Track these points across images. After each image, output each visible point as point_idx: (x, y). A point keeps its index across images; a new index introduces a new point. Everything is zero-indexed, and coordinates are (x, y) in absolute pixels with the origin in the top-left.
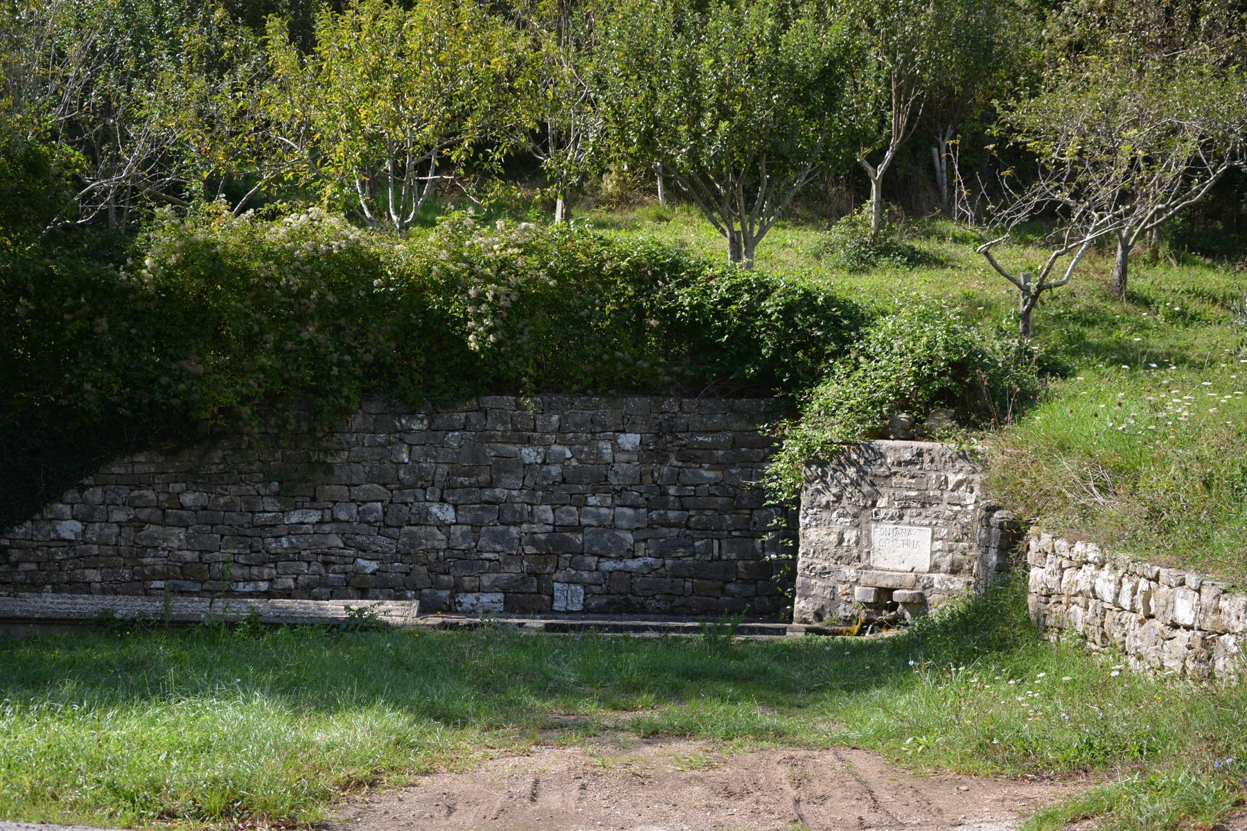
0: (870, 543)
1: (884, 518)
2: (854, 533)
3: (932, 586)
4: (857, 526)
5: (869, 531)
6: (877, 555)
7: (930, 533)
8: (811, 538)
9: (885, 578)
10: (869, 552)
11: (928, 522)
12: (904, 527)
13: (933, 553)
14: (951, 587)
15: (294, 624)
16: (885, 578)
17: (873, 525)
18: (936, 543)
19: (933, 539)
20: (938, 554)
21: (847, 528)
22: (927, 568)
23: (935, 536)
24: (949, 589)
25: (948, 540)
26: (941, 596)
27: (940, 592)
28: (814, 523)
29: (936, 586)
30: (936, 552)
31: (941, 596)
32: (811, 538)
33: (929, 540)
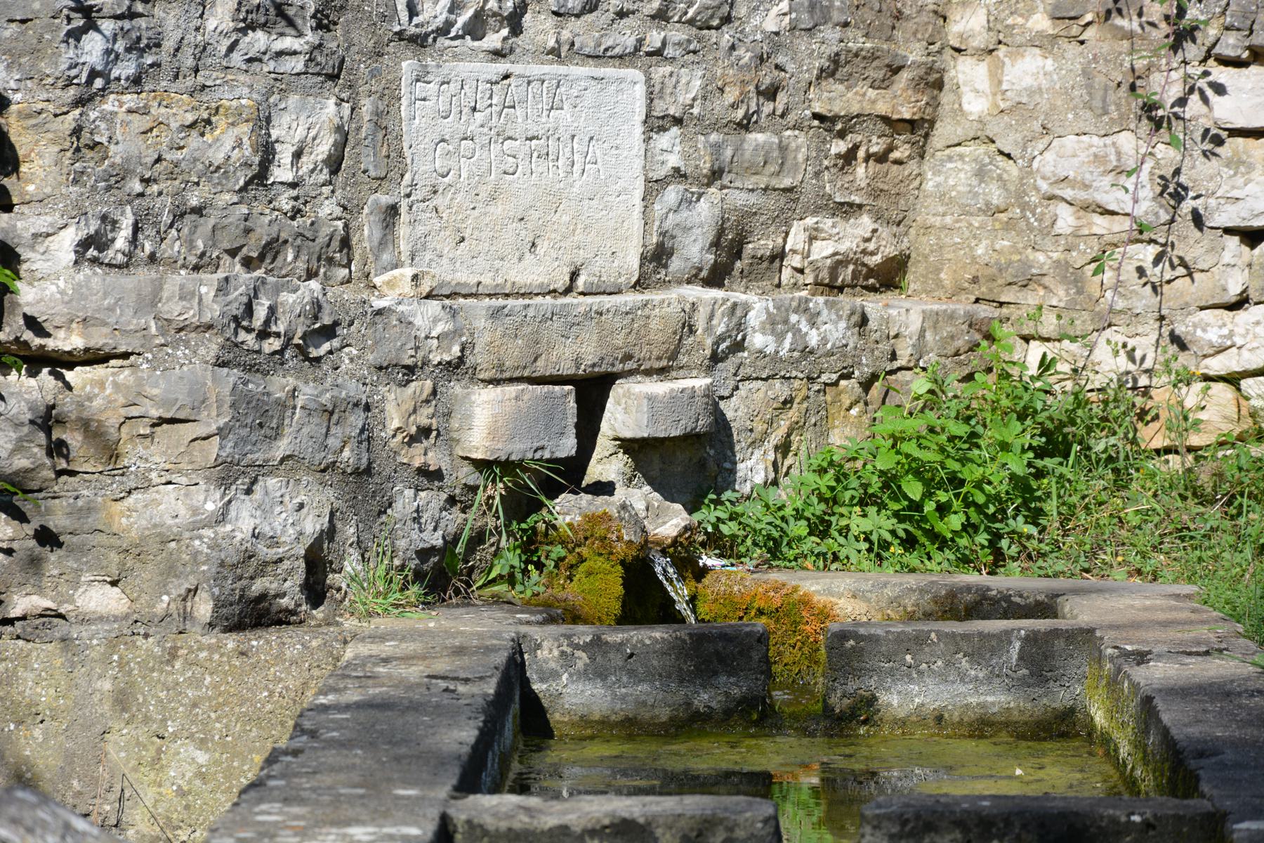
0: (395, 164)
1: (444, 31)
2: (329, 110)
3: (738, 346)
4: (334, 77)
5: (390, 95)
6: (428, 222)
7: (640, 90)
8: (117, 153)
9: (574, 324)
10: (393, 210)
11: (630, 42)
12: (536, 70)
13: (654, 187)
14: (813, 339)
15: (1139, 643)
16: (574, 324)
17: (408, 66)
18: (663, 140)
19: (655, 124)
20: (672, 194)
21: (280, 85)
22: (631, 262)
23: (660, 108)
24: (807, 352)
25: (706, 125)
26: (779, 389)
27: (772, 370)
28: (125, 69)
29: (758, 340)
30: (662, 183)
31: (779, 389)
32: (117, 153)
33: (639, 129)
